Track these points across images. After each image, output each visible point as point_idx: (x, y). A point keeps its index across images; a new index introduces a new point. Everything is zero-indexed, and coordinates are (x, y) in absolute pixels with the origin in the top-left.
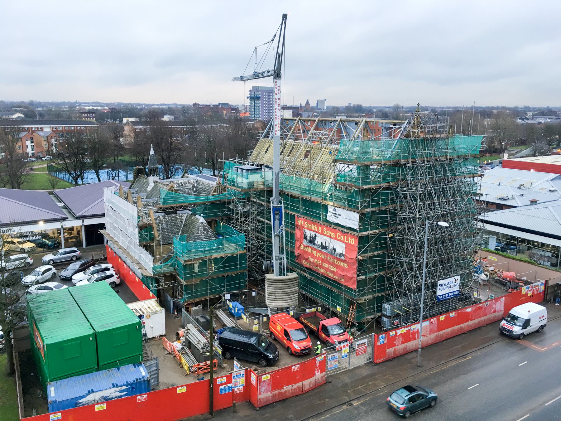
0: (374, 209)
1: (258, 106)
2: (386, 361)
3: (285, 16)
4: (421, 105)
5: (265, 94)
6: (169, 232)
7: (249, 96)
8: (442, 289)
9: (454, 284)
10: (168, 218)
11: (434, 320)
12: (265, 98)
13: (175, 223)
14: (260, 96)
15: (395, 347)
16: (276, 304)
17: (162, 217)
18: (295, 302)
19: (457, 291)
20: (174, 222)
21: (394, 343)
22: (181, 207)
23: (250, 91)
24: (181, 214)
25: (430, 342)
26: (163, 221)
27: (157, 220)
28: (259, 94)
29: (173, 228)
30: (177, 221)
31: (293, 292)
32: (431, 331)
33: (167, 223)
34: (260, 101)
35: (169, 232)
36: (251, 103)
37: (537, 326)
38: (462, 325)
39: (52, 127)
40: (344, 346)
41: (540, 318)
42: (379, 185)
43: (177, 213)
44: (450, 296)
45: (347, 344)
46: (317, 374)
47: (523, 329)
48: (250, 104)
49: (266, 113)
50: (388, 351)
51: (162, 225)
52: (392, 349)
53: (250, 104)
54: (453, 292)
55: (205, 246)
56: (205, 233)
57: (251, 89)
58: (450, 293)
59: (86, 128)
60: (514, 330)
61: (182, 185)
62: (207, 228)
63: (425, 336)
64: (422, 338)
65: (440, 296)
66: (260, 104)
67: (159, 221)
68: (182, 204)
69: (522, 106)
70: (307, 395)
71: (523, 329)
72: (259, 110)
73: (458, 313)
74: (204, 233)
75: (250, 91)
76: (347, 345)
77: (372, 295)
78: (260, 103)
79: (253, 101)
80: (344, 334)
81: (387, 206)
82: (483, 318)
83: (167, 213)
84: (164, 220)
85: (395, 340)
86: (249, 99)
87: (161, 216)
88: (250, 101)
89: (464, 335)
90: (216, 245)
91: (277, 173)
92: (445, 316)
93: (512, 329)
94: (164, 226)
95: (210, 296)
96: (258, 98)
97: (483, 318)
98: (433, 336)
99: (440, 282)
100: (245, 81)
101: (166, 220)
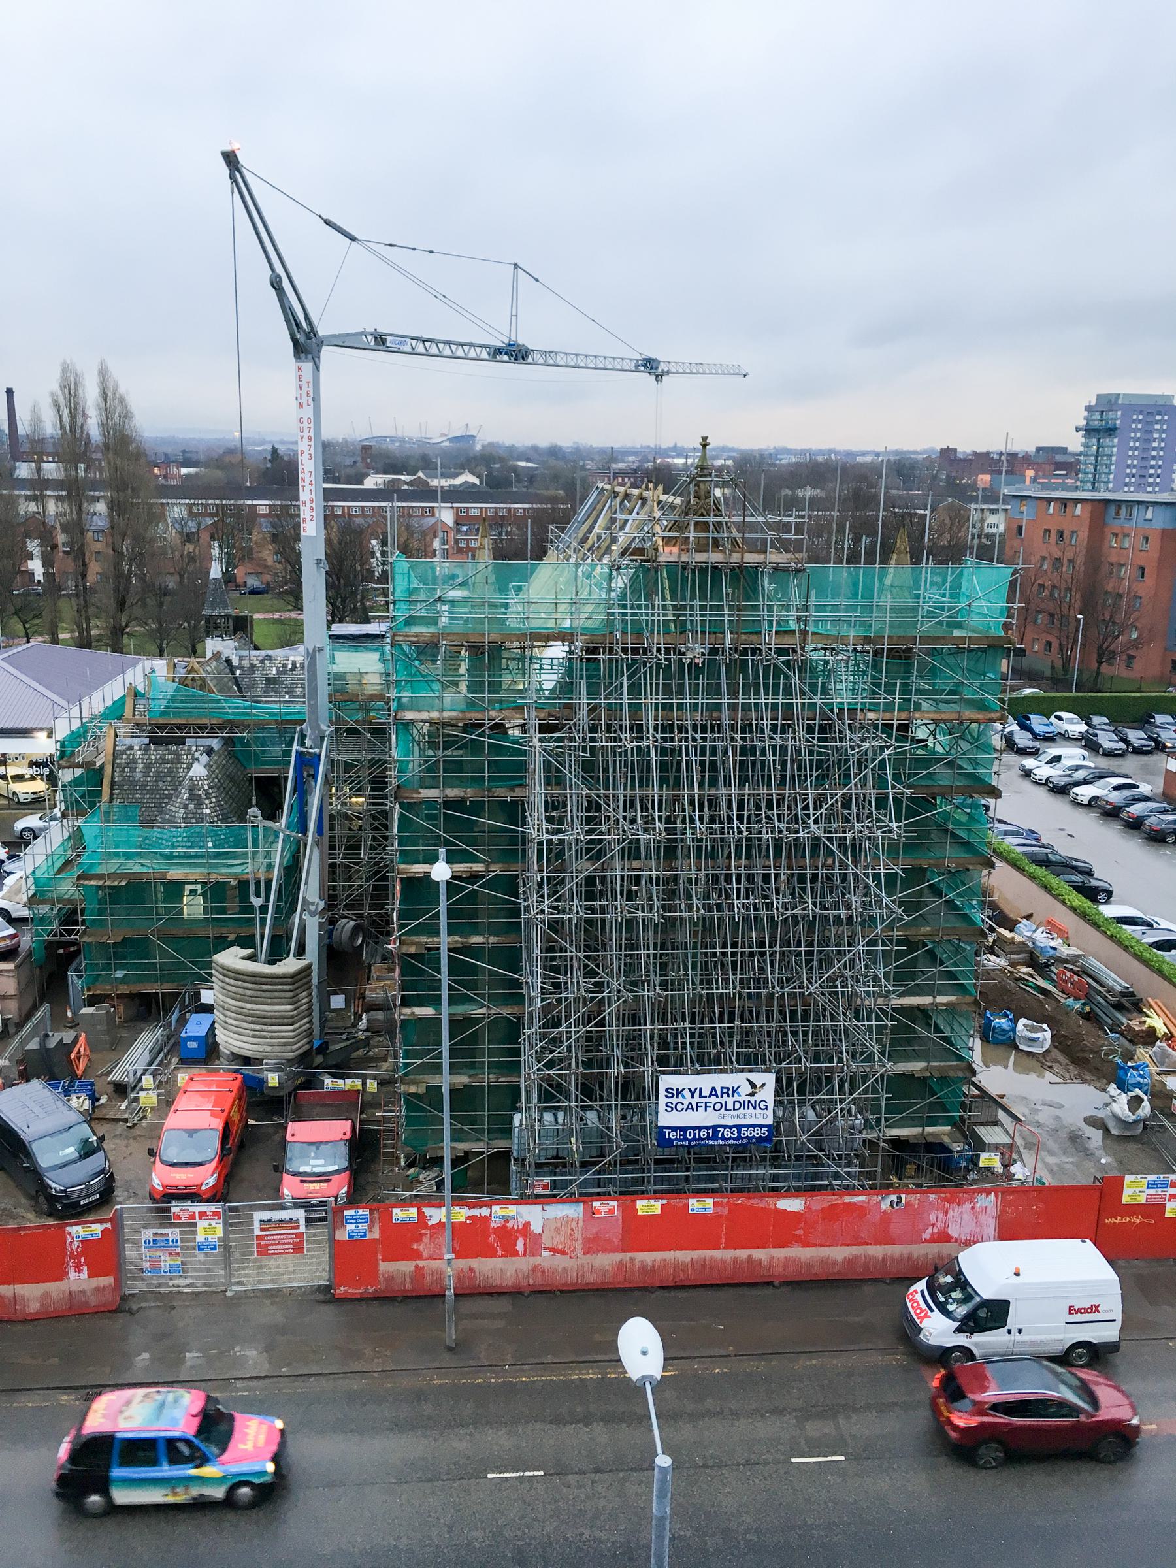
0: (462, 794)
1: (1107, 455)
2: (376, 1299)
3: (230, 159)
4: (713, 443)
5: (1135, 417)
6: (145, 792)
7: (1085, 422)
8: (679, 1107)
9: (743, 1098)
10: (154, 753)
11: (606, 1207)
12: (1136, 430)
13: (170, 771)
14: (1118, 422)
15: (421, 1263)
16: (239, 1044)
17: (140, 750)
18: (277, 1049)
19: (761, 1126)
20: (168, 766)
21: (415, 1246)
22: (202, 728)
23: (1089, 409)
24: (194, 748)
25: (590, 1278)
26: (140, 761)
27: (125, 756)
28: (1117, 418)
29: (161, 784)
30: (179, 766)
31: (271, 1018)
32: (594, 1245)
33: (148, 768)
34: (1116, 440)
35: (145, 792)
36: (1086, 445)
37: (1060, 1337)
38: (760, 1254)
39: (457, 508)
40: (202, 1215)
41: (1071, 1310)
42: (479, 716)
43: (184, 744)
44: (723, 1138)
45: (213, 1209)
46: (72, 1275)
47: (959, 1330)
48: (1082, 449)
49: (1133, 476)
50: (384, 1267)
51: (133, 770)
52: (405, 1267)
53: (1082, 449)
54: (739, 1127)
55: (176, 844)
56: (191, 806)
57: (1093, 403)
58: (725, 1127)
59: (481, 512)
60: (924, 1324)
61: (294, 668)
62: (200, 792)
63: (563, 1253)
64: (545, 1258)
65: (674, 1129)
66: (1115, 450)
67: (128, 758)
68: (205, 721)
69: (969, 450)
70: (29, 1327)
71: (959, 1330)
72: (1108, 466)
73: (733, 1209)
74: (186, 807)
75: (1089, 409)
76: (216, 1214)
77: (470, 1076)
78: (1114, 446)
79: (1095, 441)
80: (329, 1181)
81: (517, 790)
82: (877, 1251)
83: (154, 740)
84: (143, 759)
85: (419, 1239)
86: (1082, 433)
87: (136, 748)
88: (1083, 440)
89: (768, 1291)
90: (210, 844)
91: (311, 651)
92: (664, 1202)
93: (922, 1319)
94: (138, 775)
95: (165, 986)
96: (1111, 431)
97: (877, 1251)
98: (606, 1261)
99: (668, 1081)
100: (659, 377)
101: (149, 758)
